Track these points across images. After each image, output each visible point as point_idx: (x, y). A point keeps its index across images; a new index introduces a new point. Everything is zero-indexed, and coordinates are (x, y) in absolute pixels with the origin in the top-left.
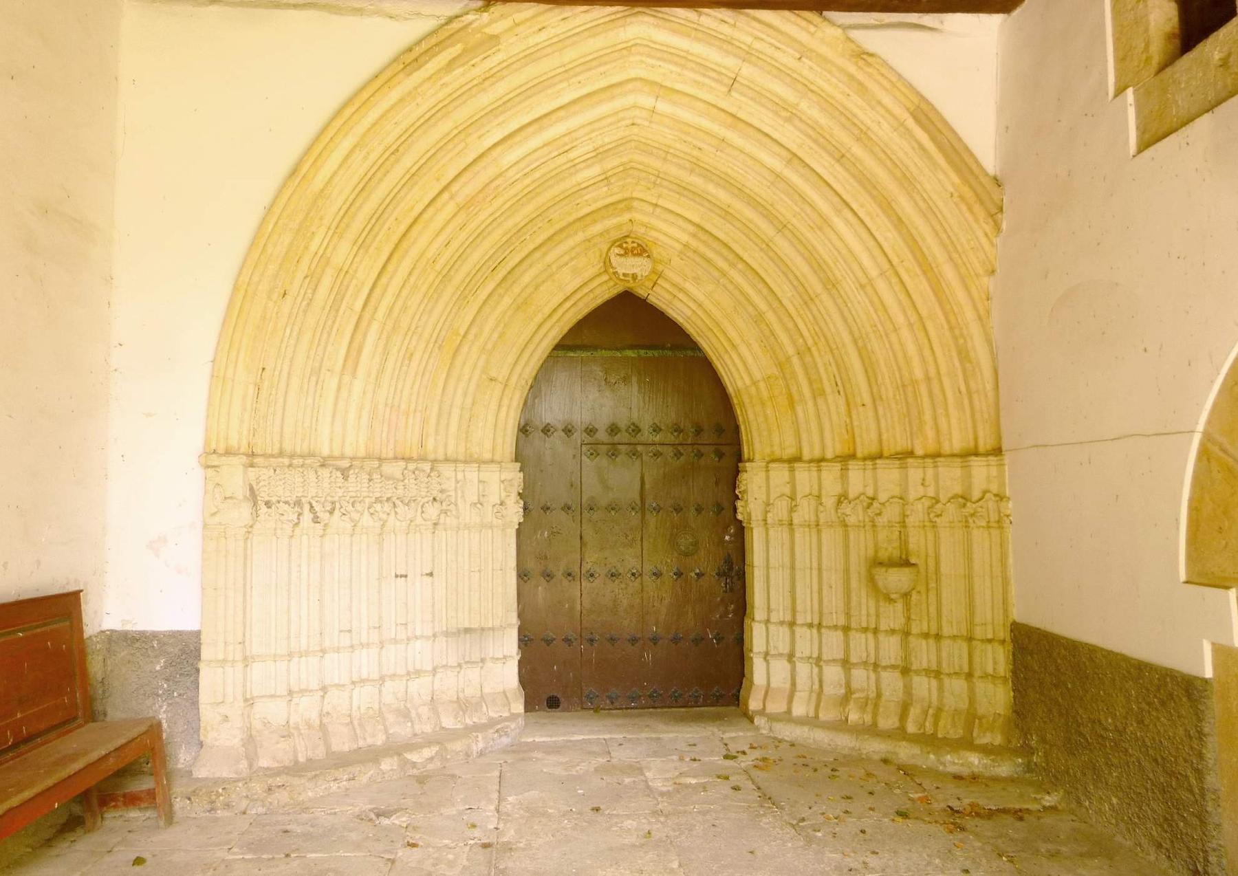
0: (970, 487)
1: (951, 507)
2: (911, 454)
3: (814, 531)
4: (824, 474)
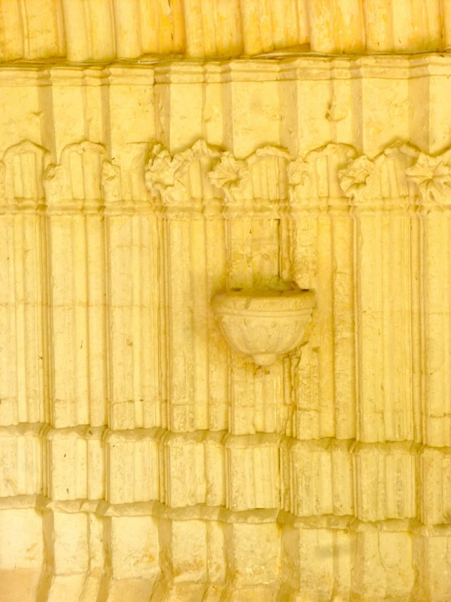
0: (425, 120)
1: (388, 168)
2: (305, 48)
3: (94, 221)
4: (116, 92)
